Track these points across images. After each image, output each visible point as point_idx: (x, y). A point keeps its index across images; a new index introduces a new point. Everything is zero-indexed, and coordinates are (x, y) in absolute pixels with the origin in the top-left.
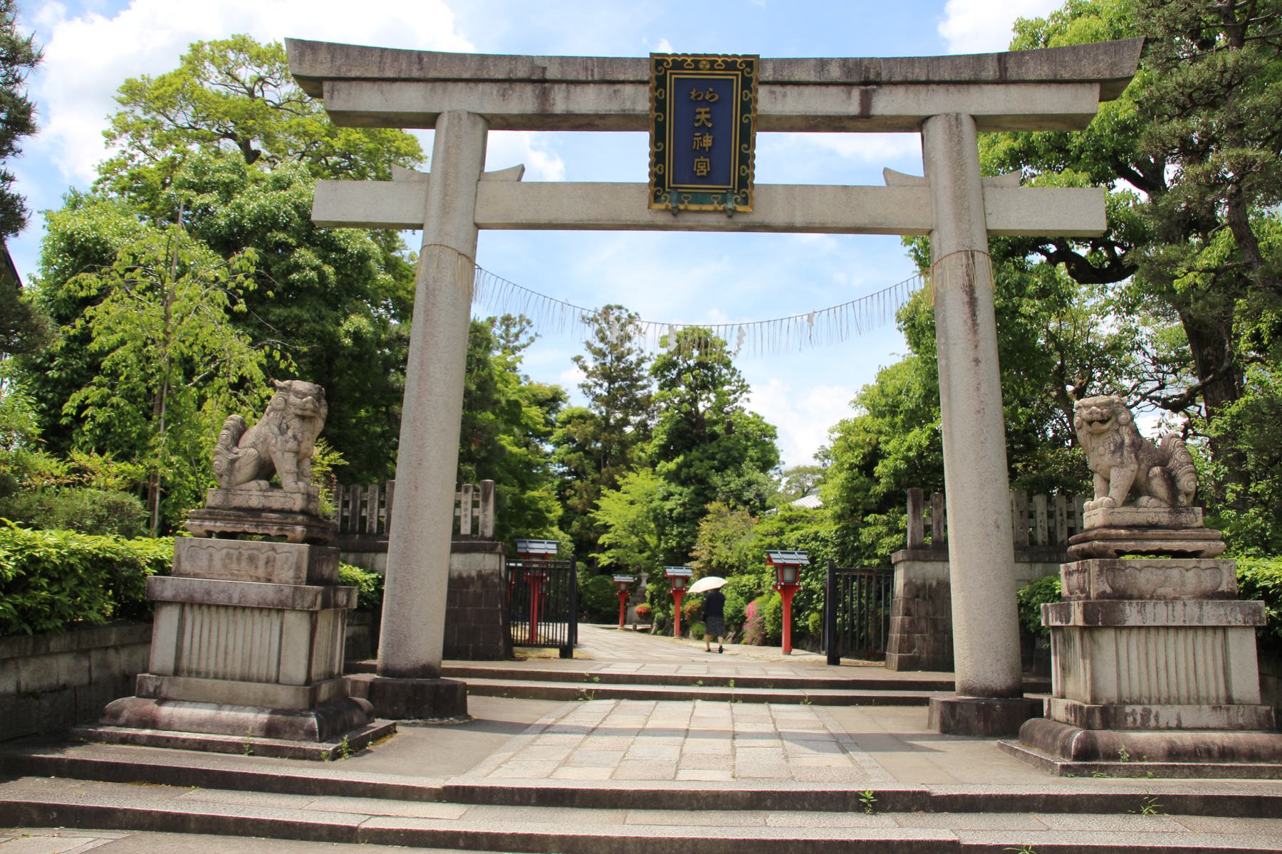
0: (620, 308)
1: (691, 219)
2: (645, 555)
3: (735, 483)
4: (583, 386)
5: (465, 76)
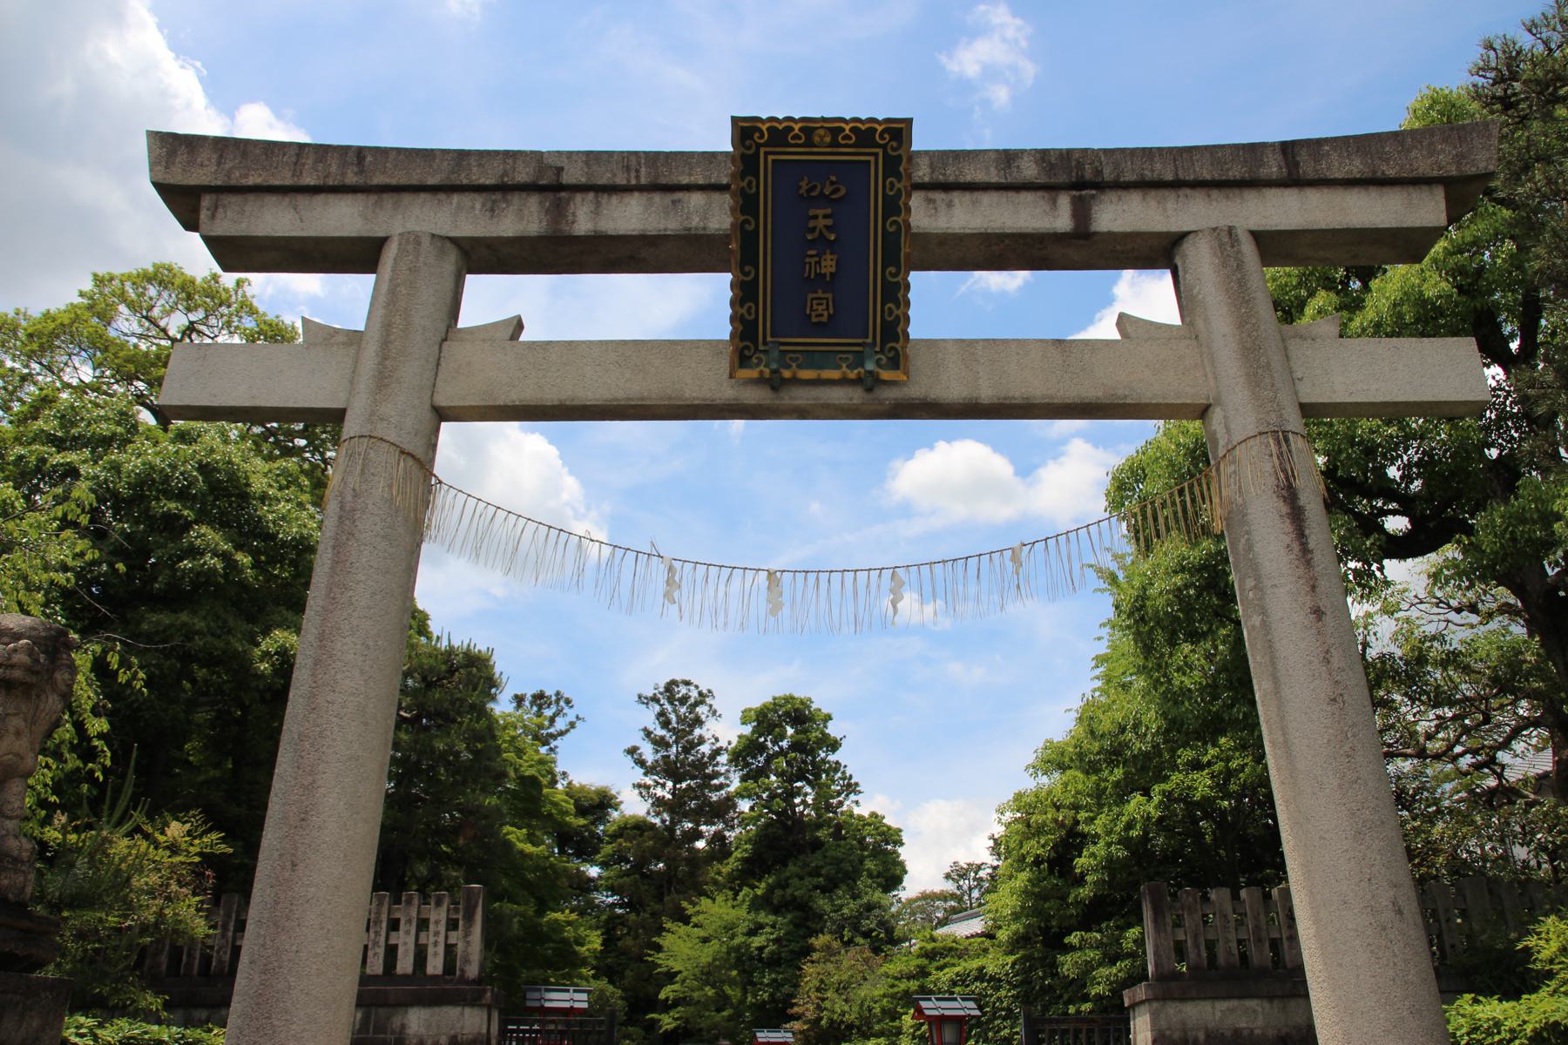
0: (687, 683)
1: (802, 396)
2: (725, 1013)
3: (850, 908)
4: (639, 786)
5: (431, 181)
